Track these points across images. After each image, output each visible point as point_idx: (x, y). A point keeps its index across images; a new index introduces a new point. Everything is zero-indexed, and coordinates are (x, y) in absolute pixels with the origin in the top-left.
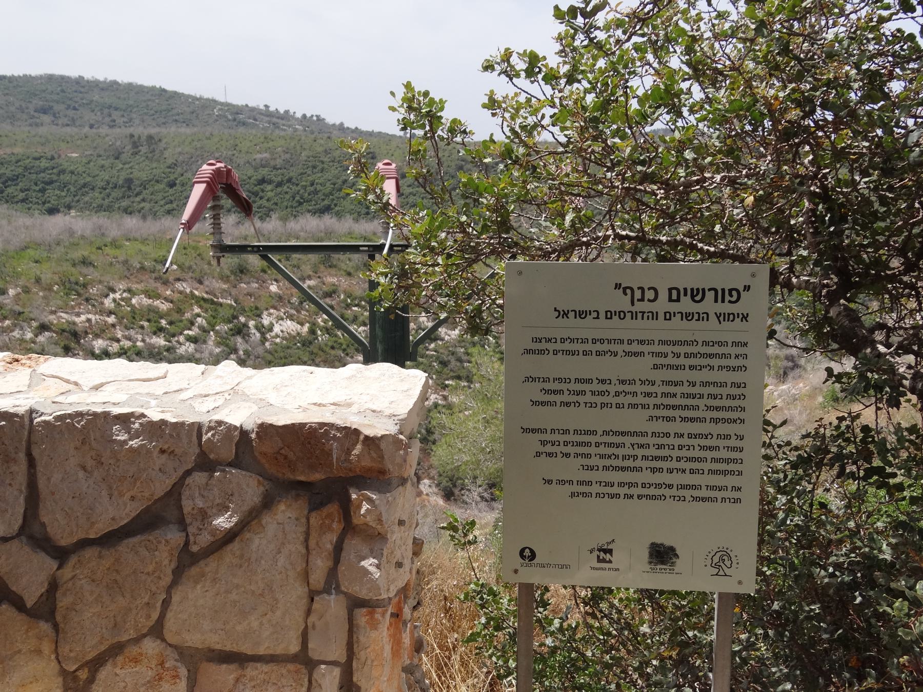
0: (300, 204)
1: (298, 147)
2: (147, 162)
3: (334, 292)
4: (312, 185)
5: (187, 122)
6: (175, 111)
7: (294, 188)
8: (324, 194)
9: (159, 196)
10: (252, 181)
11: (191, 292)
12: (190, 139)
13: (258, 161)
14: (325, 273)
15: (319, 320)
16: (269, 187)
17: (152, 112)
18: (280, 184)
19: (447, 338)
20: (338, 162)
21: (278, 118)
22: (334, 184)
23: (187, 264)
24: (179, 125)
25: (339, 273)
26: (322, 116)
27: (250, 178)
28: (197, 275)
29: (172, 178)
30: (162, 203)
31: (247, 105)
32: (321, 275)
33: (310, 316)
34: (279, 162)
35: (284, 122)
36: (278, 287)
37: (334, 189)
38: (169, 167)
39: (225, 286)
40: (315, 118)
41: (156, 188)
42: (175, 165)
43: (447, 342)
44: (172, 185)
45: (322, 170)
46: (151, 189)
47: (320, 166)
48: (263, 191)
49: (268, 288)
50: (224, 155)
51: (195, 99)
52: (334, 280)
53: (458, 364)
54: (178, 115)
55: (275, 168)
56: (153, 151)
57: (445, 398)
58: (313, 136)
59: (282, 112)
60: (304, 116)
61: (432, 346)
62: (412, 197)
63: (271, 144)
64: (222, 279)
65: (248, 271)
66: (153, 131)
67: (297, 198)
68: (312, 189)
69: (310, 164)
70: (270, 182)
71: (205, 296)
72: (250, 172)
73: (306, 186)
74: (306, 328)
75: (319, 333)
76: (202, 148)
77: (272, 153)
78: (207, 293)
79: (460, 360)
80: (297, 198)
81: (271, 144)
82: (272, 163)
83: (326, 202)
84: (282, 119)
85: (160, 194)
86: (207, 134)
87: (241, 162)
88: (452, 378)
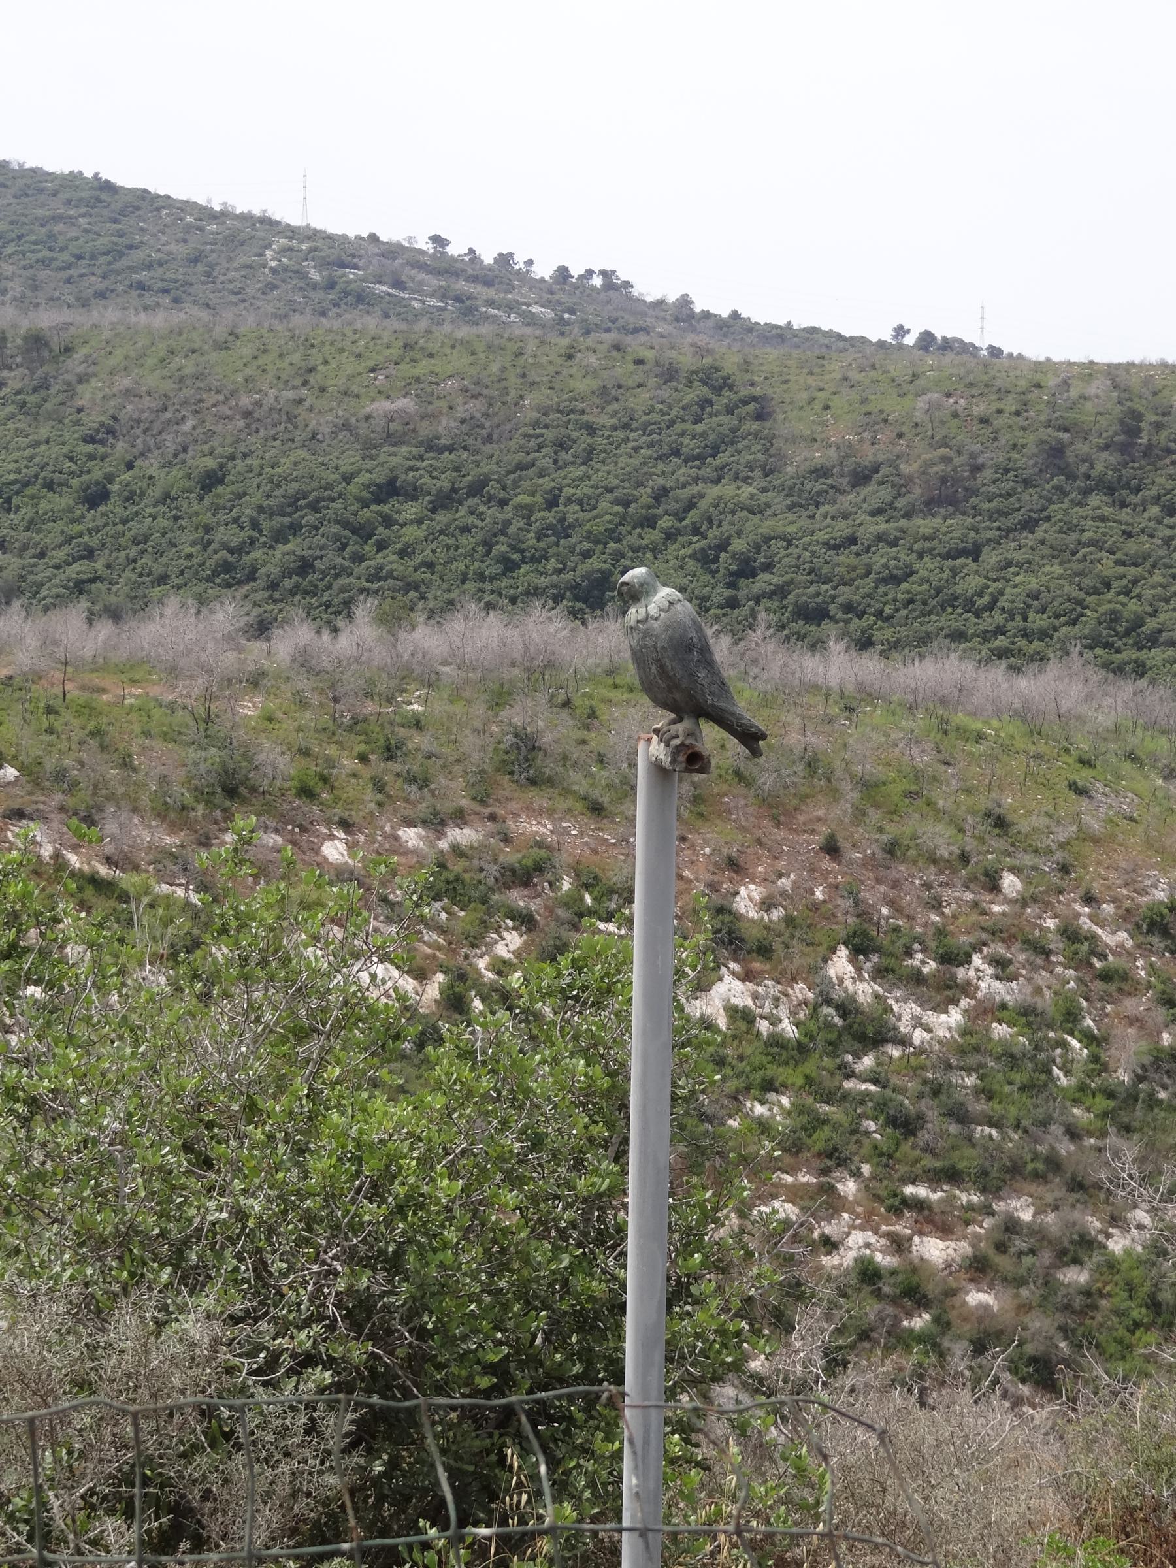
0: (510, 567)
1: (513, 379)
2: (21, 423)
3: (539, 868)
4: (552, 503)
5: (176, 294)
6: (139, 255)
7: (493, 514)
8: (589, 537)
9: (53, 533)
10: (354, 488)
11: (57, 856)
12: (161, 348)
13: (379, 423)
14: (514, 806)
15: (482, 964)
16: (410, 510)
17: (66, 257)
18: (445, 501)
19: (919, 1036)
20: (644, 428)
21: (474, 279)
22: (626, 504)
23: (50, 764)
24: (149, 299)
25: (561, 805)
26: (623, 276)
27: (347, 479)
28: (81, 799)
29: (97, 475)
30: (61, 555)
31: (373, 238)
32: (501, 812)
33: (451, 948)
34: (446, 427)
35: (492, 293)
36: (352, 846)
37: (623, 517)
38: (90, 440)
39: (170, 840)
40: (597, 281)
41: (44, 505)
42: (111, 432)
43: (921, 1051)
44: (96, 497)
45: (589, 456)
46: (27, 512)
47: (584, 441)
48: (388, 521)
49: (316, 851)
50: (270, 401)
51: (206, 214)
52: (543, 828)
53: (954, 1128)
54: (149, 267)
55: (431, 446)
56: (44, 385)
57: (899, 1245)
58: (564, 342)
59: (488, 259)
60: (563, 273)
61: (868, 1061)
62: (884, 549)
63: (424, 367)
64: (161, 816)
65: (253, 790)
66: (46, 319)
67: (500, 548)
68: (551, 517)
69: (549, 434)
70: (413, 493)
71: (103, 871)
72: (350, 460)
73: (530, 509)
74: (433, 990)
75: (478, 1005)
76: (197, 377)
77: (425, 398)
78: (108, 861)
79: (959, 1115)
80: (500, 548)
81: (424, 367)
82: (425, 429)
83: (595, 563)
84: (488, 283)
85: (59, 526)
86: (220, 332)
87: (323, 424)
88: (935, 1178)
